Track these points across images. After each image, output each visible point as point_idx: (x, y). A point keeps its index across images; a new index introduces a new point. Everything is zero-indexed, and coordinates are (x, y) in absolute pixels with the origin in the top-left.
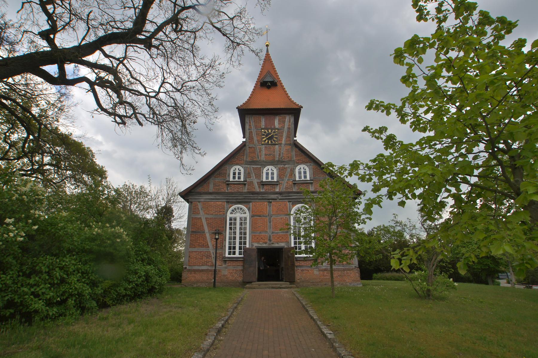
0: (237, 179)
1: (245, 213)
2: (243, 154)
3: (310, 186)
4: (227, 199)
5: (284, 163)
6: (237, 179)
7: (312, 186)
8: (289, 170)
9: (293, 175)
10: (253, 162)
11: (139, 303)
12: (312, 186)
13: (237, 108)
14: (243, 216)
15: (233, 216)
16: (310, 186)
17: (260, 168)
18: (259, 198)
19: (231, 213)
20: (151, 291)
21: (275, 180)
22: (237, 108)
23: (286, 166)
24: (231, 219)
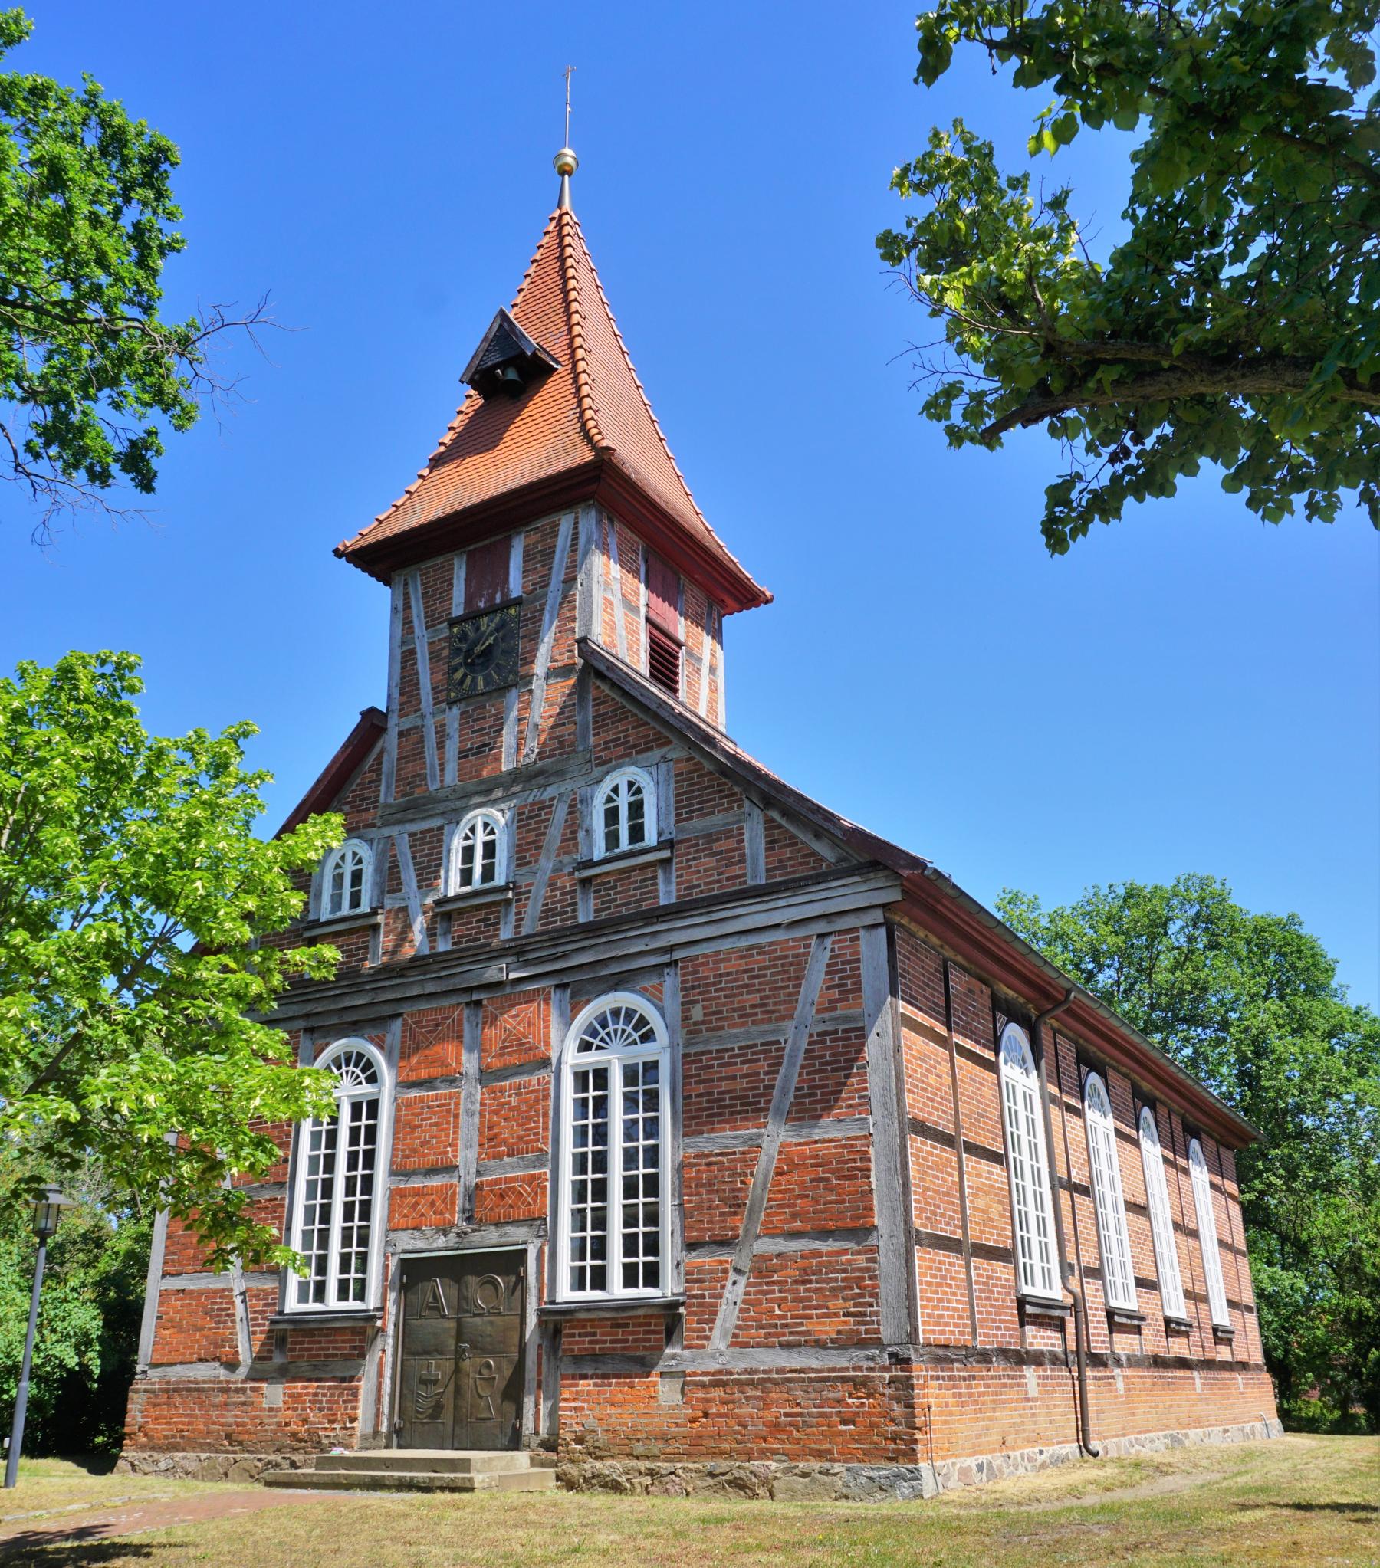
0: (624, 845)
1: (648, 1037)
2: (374, 776)
3: (660, 874)
4: (307, 1016)
5: (541, 780)
6: (624, 845)
7: (667, 872)
8: (560, 812)
9: (581, 834)
10: (413, 807)
11: (123, 1454)
12: (667, 872)
13: (1016, 85)
14: (644, 1053)
15: (593, 1058)
16: (660, 874)
17: (441, 828)
18: (430, 988)
19: (585, 1047)
20: (703, 1521)
21: (500, 880)
22: (1016, 85)
23: (551, 792)
24: (581, 1079)
